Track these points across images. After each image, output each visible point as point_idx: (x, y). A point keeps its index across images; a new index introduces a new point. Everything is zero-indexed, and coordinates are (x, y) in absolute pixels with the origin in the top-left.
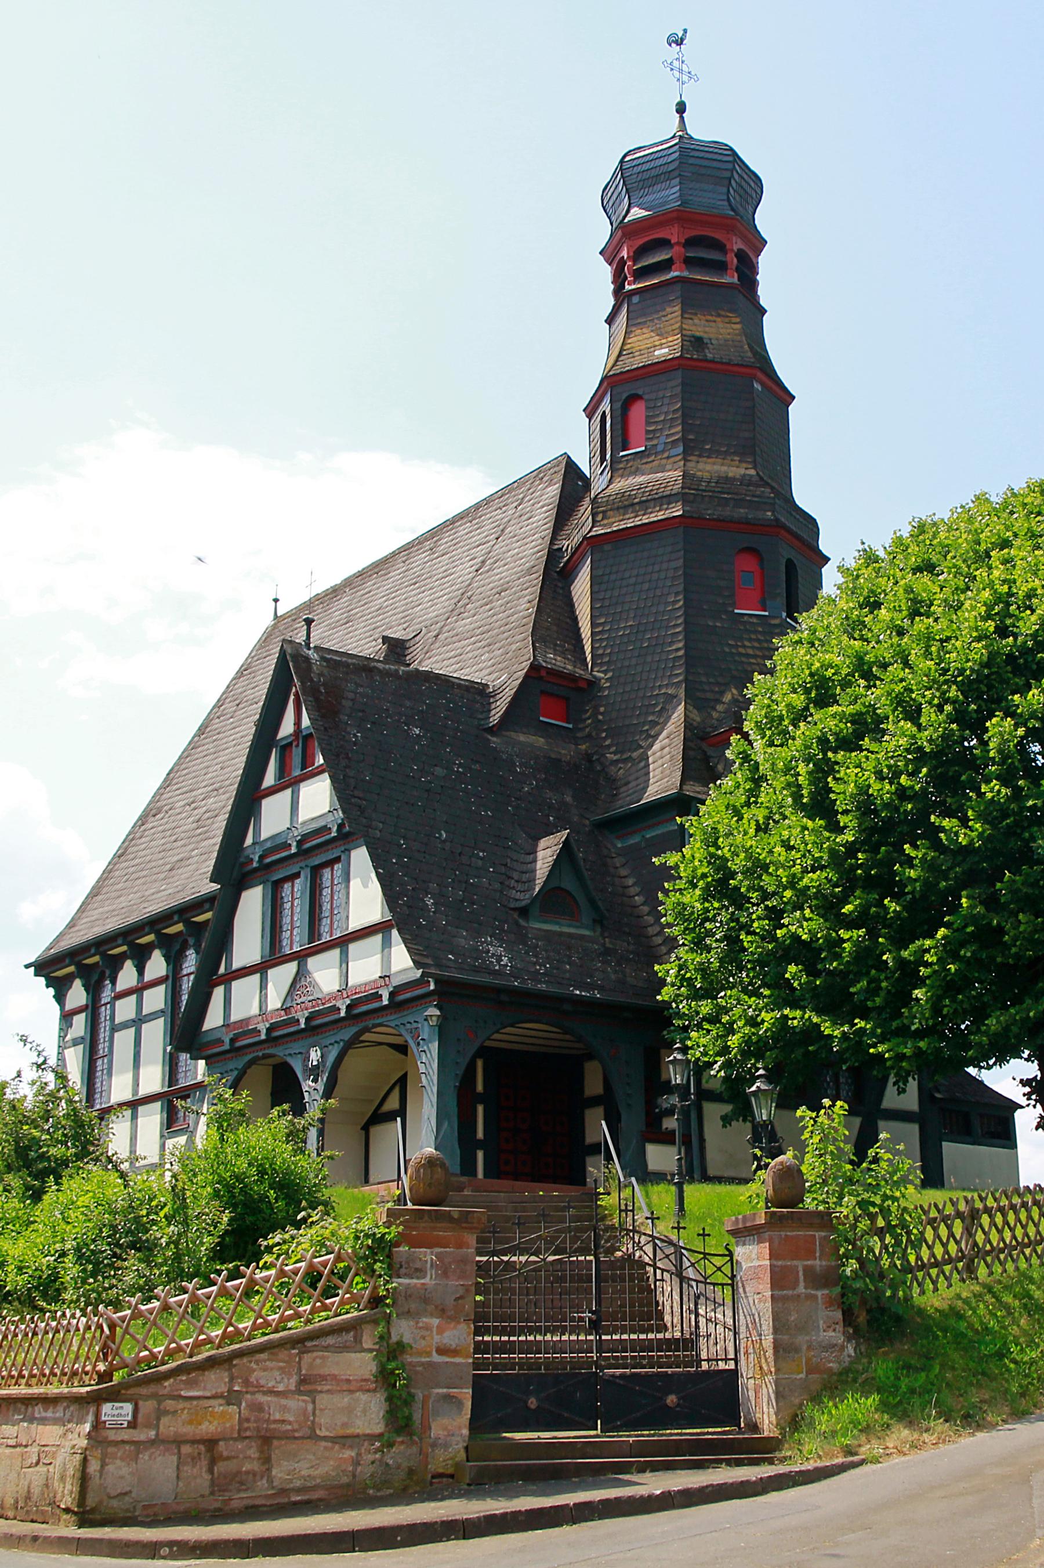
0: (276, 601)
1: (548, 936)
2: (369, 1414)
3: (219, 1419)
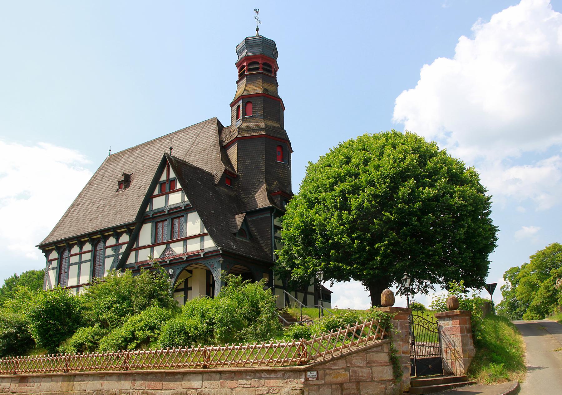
0: (110, 150)
1: (241, 241)
2: (388, 373)
3: (343, 376)
